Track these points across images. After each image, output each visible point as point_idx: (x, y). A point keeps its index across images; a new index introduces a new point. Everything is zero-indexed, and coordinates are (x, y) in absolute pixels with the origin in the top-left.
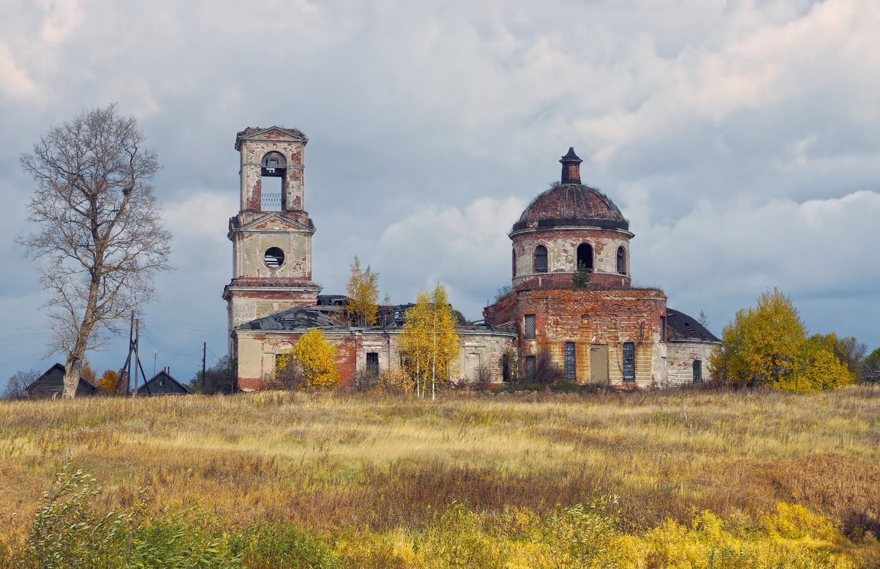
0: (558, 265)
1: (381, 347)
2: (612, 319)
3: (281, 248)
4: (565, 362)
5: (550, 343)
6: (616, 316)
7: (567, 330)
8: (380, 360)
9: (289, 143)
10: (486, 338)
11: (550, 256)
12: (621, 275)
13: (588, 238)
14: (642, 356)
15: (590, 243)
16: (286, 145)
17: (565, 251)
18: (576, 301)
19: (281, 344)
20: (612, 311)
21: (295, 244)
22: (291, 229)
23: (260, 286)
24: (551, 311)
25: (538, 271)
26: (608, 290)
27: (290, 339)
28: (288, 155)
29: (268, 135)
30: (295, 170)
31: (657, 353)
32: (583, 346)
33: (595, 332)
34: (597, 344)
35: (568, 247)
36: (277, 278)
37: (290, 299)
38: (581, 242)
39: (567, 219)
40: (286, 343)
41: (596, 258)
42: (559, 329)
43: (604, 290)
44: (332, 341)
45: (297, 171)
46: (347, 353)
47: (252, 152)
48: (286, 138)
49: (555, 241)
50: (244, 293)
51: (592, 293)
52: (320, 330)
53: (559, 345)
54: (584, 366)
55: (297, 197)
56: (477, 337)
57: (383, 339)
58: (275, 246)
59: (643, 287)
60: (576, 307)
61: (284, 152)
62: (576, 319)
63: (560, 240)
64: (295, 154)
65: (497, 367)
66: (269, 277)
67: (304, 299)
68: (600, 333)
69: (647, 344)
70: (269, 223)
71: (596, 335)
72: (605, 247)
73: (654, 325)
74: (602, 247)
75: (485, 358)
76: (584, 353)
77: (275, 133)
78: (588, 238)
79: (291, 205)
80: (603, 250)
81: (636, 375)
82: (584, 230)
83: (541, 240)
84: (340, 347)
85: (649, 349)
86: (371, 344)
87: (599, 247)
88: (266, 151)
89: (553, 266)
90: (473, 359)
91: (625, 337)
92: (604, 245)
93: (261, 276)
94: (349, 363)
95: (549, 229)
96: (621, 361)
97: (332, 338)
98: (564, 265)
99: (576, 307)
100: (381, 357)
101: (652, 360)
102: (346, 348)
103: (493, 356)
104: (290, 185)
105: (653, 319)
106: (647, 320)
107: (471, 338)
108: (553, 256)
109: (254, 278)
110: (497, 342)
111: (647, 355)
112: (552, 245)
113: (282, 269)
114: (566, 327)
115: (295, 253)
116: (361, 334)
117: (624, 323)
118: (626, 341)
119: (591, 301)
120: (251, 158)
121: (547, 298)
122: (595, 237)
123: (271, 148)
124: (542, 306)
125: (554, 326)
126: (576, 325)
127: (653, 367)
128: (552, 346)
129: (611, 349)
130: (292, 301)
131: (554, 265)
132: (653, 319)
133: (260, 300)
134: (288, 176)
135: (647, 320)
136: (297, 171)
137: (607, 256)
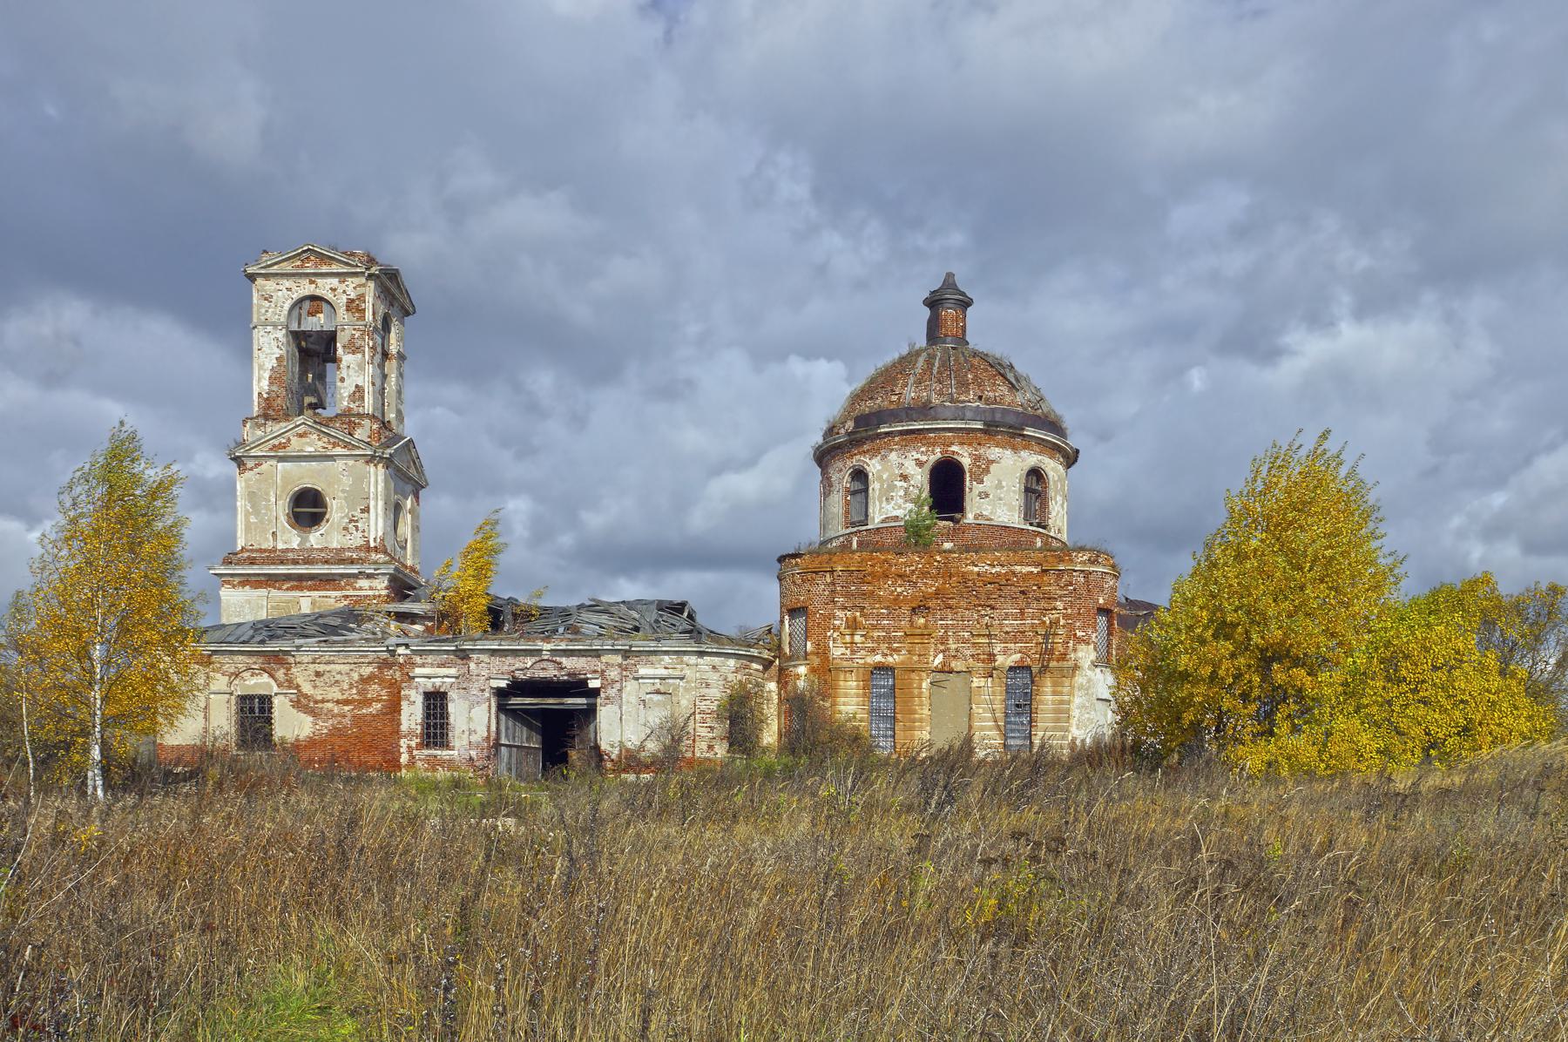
0: (889, 507)
1: (453, 680)
3: (320, 489)
6: (993, 608)
7: (878, 640)
8: (451, 708)
9: (341, 276)
10: (686, 658)
11: (873, 489)
12: (1034, 529)
13: (954, 448)
15: (959, 458)
16: (334, 282)
17: (904, 478)
18: (900, 576)
19: (246, 675)
20: (983, 597)
21: (347, 482)
22: (339, 451)
23: (274, 564)
25: (853, 524)
26: (976, 552)
27: (263, 664)
29: (299, 263)
30: (354, 332)
31: (1086, 689)
32: (914, 676)
33: (942, 644)
34: (945, 670)
35: (910, 468)
36: (312, 549)
37: (335, 590)
38: (939, 455)
39: (910, 408)
40: (257, 672)
41: (972, 490)
42: (857, 639)
43: (968, 552)
45: (357, 334)
46: (383, 693)
47: (268, 298)
48: (335, 268)
49: (884, 458)
50: (242, 579)
51: (938, 558)
54: (915, 718)
55: (357, 386)
56: (666, 658)
57: (459, 661)
58: (309, 486)
60: (899, 590)
61: (330, 296)
62: (898, 616)
63: (894, 453)
64: (352, 301)
66: (296, 547)
67: (361, 589)
68: (953, 646)
70: (294, 440)
71: (943, 651)
72: (993, 468)
73: (1082, 628)
74: (988, 467)
75: (684, 702)
76: (916, 691)
77: (312, 258)
78: (954, 448)
79: (346, 403)
81: (1033, 737)
82: (944, 429)
83: (858, 457)
85: (1067, 682)
86: (430, 674)
87: (979, 467)
88: (296, 296)
89: (880, 512)
90: (658, 704)
91: (1011, 655)
92: (993, 462)
93: (280, 546)
95: (871, 433)
96: (999, 706)
97: (350, 661)
98: (900, 507)
99: (899, 590)
100: (453, 701)
101: (1073, 706)
102: (382, 681)
103: (703, 698)
104: (344, 364)
105: (1079, 614)
108: (880, 490)
109: (265, 551)
110: (714, 667)
111: (1061, 694)
113: (320, 532)
116: (408, 652)
117: (1011, 624)
118: (1012, 664)
119: (935, 578)
120: (267, 311)
121: (832, 572)
123: (306, 289)
124: (821, 586)
125: (847, 631)
126: (899, 629)
127: (1074, 722)
129: (977, 682)
130: (338, 593)
131: (881, 508)
132: (1079, 614)
133: (274, 592)
134: (338, 345)
135: (1066, 616)
136: (357, 334)
137: (999, 486)
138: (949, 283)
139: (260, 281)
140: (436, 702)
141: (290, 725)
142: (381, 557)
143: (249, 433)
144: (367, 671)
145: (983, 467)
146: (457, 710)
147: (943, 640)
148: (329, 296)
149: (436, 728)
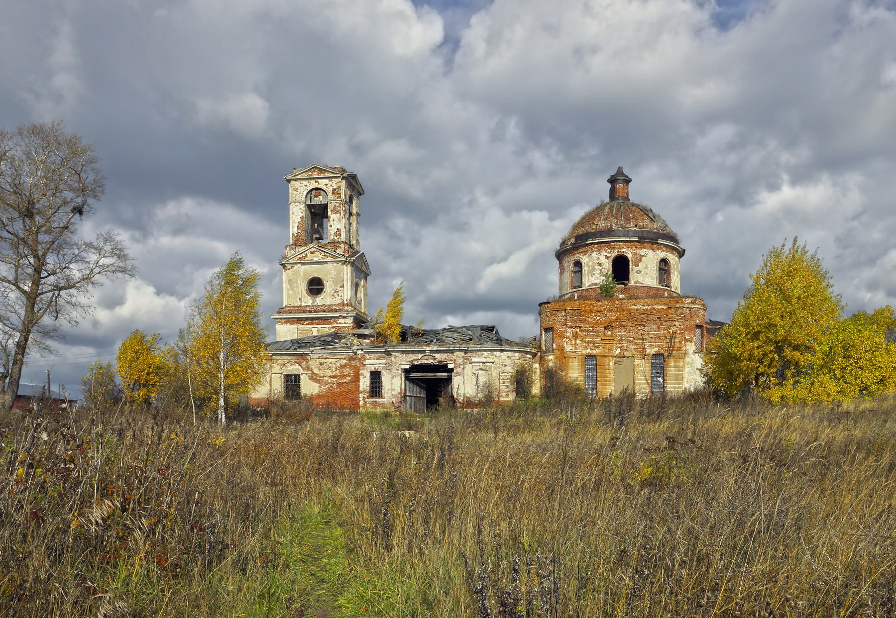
0: (593, 279)
2: (639, 330)
4: (585, 377)
5: (568, 357)
6: (644, 326)
7: (588, 343)
8: (383, 378)
10: (495, 353)
13: (624, 250)
14: (673, 368)
15: (626, 255)
16: (327, 181)
17: (600, 264)
19: (288, 365)
20: (639, 321)
21: (333, 273)
22: (329, 259)
24: (569, 324)
28: (330, 190)
29: (310, 173)
32: (606, 359)
33: (620, 343)
34: (621, 356)
35: (603, 260)
37: (328, 324)
38: (617, 253)
39: (602, 231)
41: (633, 270)
42: (578, 342)
44: (337, 360)
45: (337, 205)
48: (327, 175)
51: (617, 303)
52: (323, 350)
53: (578, 359)
55: (337, 229)
56: (485, 353)
57: (387, 357)
59: (560, 242)
60: (598, 318)
63: (594, 253)
64: (335, 189)
65: (507, 383)
67: (340, 323)
68: (625, 345)
69: (678, 354)
72: (643, 259)
73: (688, 335)
74: (641, 259)
75: (494, 374)
76: (607, 367)
78: (624, 250)
80: (641, 261)
83: (577, 255)
84: (345, 366)
85: (681, 361)
86: (374, 362)
88: (309, 189)
92: (643, 256)
93: (303, 304)
94: (352, 382)
96: (648, 373)
98: (598, 278)
99: (598, 318)
100: (384, 375)
101: (685, 373)
102: (350, 367)
103: (503, 372)
104: (331, 219)
106: (680, 329)
107: (479, 353)
108: (588, 271)
109: (296, 307)
110: (508, 357)
112: (587, 260)
114: (587, 340)
115: (333, 281)
116: (362, 352)
118: (654, 353)
119: (616, 312)
121: (565, 310)
122: (632, 248)
123: (314, 185)
125: (573, 339)
127: (685, 380)
128: (571, 360)
129: (637, 362)
133: (300, 326)
135: (680, 329)
136: (337, 205)
137: (646, 268)
138: (620, 171)
139: (292, 182)
140: (376, 376)
141: (308, 388)
142: (350, 308)
143: (289, 253)
144: (344, 362)
145: (638, 259)
146: (385, 379)
147: (620, 342)
148: (324, 188)
149: (376, 389)
